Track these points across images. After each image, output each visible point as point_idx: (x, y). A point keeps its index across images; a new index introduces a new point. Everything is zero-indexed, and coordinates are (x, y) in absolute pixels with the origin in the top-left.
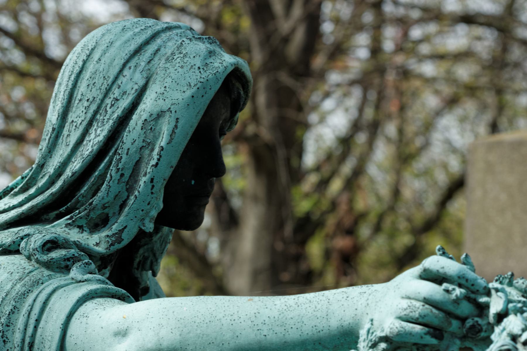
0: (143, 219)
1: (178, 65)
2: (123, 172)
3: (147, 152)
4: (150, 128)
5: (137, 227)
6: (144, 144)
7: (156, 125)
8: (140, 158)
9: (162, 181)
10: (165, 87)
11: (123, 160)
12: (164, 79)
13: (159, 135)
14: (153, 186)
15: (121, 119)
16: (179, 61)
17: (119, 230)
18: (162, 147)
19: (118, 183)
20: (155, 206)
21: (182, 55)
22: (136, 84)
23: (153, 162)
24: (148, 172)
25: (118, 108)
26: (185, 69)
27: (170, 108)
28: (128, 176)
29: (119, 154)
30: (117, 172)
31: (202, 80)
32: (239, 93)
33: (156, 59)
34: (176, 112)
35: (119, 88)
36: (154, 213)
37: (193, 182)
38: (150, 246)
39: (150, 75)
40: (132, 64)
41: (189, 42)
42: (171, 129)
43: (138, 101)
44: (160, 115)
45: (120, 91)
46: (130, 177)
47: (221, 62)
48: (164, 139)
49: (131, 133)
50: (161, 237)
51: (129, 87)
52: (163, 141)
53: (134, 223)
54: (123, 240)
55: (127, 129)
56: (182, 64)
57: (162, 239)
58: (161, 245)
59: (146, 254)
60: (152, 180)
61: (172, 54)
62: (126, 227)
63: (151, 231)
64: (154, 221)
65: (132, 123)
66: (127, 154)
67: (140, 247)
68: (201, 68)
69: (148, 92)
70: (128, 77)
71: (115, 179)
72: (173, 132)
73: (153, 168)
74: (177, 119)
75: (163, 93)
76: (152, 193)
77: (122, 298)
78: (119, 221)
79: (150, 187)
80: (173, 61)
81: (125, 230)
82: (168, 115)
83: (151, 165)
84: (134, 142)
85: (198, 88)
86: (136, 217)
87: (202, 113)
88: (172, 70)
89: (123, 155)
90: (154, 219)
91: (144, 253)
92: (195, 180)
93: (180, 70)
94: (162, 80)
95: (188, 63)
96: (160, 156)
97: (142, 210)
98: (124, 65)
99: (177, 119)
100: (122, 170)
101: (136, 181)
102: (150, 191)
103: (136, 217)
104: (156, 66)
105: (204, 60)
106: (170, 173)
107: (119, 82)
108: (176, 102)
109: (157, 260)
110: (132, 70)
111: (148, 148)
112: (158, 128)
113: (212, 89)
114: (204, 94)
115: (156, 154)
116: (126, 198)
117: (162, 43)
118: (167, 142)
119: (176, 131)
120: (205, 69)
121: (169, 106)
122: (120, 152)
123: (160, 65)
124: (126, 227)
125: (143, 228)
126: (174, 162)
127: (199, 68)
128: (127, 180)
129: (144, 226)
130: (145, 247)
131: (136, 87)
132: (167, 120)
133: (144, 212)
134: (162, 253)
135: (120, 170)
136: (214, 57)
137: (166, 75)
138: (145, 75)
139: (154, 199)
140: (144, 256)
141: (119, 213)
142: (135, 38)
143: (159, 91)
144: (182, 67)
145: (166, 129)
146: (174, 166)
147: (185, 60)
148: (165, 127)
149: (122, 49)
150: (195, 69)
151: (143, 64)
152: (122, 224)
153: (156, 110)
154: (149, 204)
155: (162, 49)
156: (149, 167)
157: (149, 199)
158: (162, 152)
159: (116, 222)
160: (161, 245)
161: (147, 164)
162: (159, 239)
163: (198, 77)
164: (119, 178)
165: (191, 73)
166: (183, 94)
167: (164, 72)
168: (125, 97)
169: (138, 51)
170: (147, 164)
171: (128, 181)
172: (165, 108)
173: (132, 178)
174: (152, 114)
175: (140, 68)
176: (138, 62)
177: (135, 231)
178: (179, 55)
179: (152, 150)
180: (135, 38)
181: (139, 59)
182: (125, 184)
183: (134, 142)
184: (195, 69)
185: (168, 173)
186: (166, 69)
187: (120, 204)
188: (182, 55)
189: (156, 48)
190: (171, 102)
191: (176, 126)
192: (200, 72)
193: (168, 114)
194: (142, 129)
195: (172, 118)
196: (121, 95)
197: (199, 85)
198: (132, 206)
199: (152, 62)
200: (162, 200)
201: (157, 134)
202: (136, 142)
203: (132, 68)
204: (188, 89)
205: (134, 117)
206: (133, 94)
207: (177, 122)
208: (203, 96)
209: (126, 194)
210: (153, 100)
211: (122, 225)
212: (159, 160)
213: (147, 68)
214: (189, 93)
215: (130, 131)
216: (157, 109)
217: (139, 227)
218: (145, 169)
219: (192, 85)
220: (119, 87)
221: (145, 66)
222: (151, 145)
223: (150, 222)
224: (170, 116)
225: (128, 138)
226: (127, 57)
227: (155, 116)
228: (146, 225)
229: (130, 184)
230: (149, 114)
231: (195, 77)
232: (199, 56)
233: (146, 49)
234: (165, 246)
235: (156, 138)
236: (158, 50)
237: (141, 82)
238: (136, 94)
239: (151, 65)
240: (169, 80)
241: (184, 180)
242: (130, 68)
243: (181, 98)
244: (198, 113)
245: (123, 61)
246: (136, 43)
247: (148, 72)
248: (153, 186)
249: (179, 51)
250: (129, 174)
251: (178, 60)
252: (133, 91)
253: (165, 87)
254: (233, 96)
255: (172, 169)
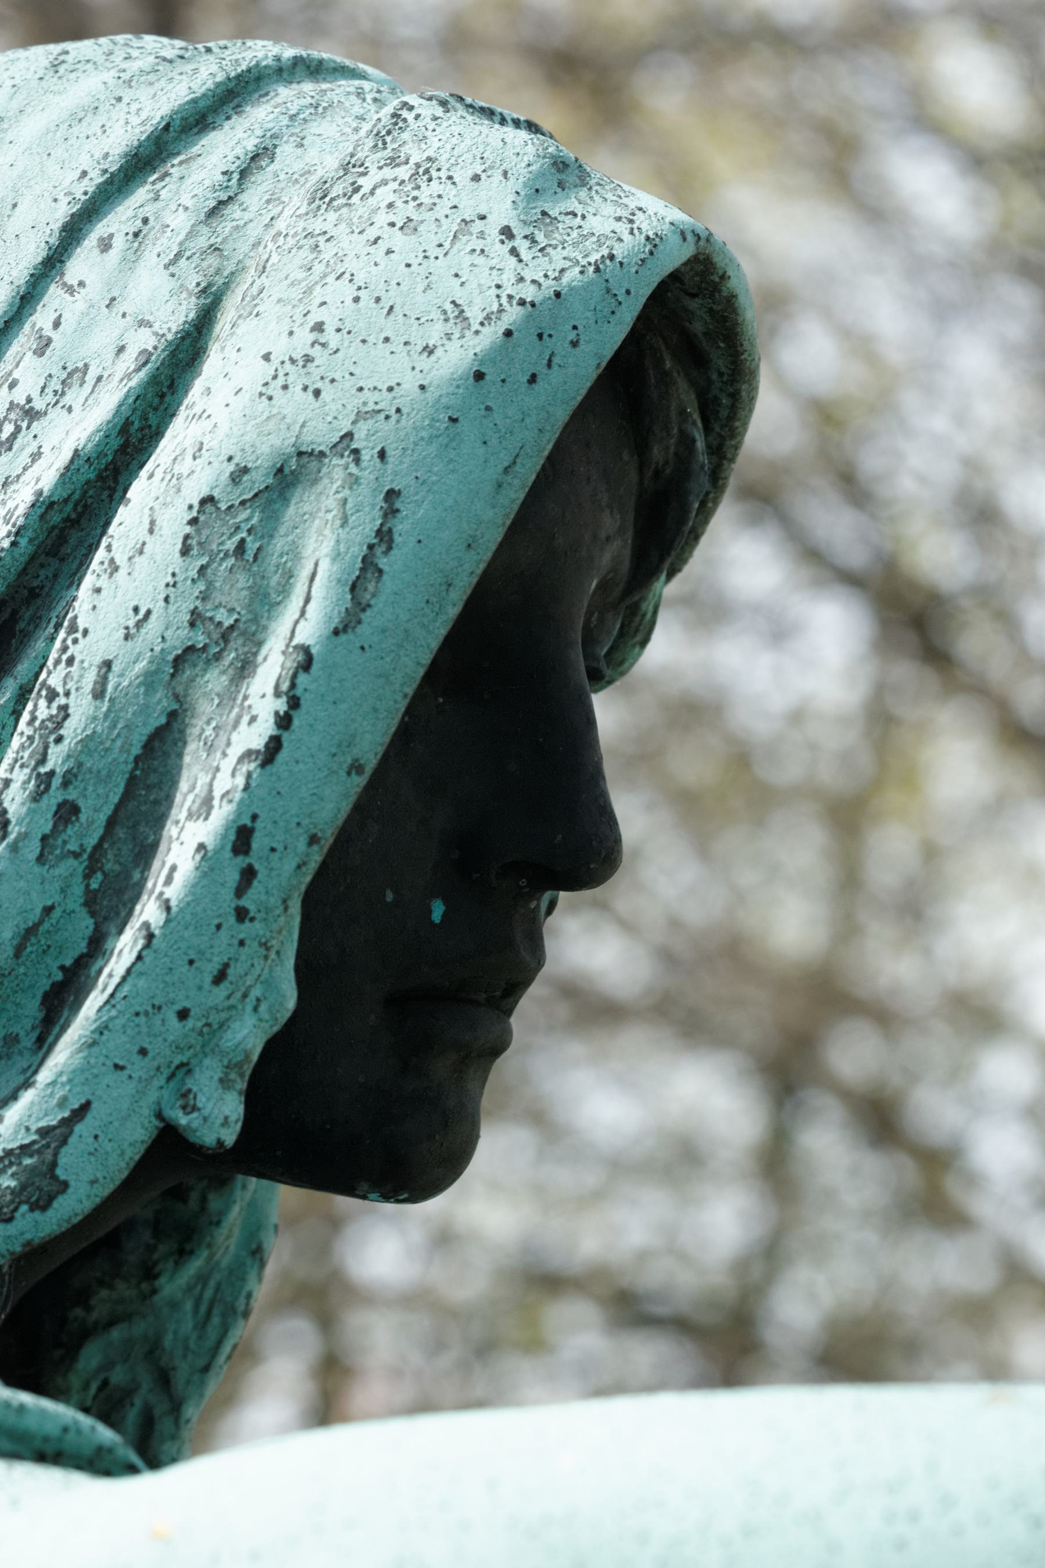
0: (185, 1068)
1: (382, 218)
2: (72, 794)
3: (215, 680)
4: (231, 545)
5: (146, 1111)
6: (200, 639)
7: (268, 528)
8: (173, 715)
9: (302, 845)
10: (319, 327)
11: (72, 729)
12: (308, 291)
13: (285, 589)
14: (249, 874)
15: (56, 518)
16: (391, 198)
17: (44, 1132)
18: (306, 650)
19: (41, 859)
20: (256, 992)
21: (404, 172)
22: (143, 323)
23: (254, 736)
24: (217, 794)
25: (36, 456)
26: (428, 237)
27: (349, 436)
28: (102, 818)
29: (52, 695)
30: (37, 797)
31: (529, 293)
32: (685, 441)
33: (253, 197)
34: (382, 455)
35: (40, 352)
36: (249, 1035)
37: (438, 911)
38: (139, 1328)
39: (220, 281)
40: (117, 221)
41: (439, 111)
42: (358, 551)
43: (153, 420)
44: (288, 476)
45: (51, 363)
46: (111, 823)
47: (625, 214)
48: (311, 608)
49: (122, 572)
50: (202, 1279)
51: (107, 332)
52: (304, 618)
53: (130, 1088)
54: (65, 1185)
55: (100, 554)
56: (404, 211)
57: (208, 1294)
58: (202, 1325)
59: (118, 1376)
60: (242, 838)
61: (346, 168)
62: (85, 1107)
63: (230, 1137)
64: (242, 1085)
65: (127, 523)
66: (98, 694)
67: (86, 1334)
68: (518, 231)
69: (212, 365)
70: (95, 291)
71: (23, 837)
72: (369, 565)
73: (252, 766)
74: (391, 495)
75: (308, 359)
76: (242, 914)
77: (99, 1464)
78: (44, 1076)
79: (233, 877)
80: (356, 198)
81: (79, 1128)
82: (339, 475)
83: (235, 751)
84: (139, 625)
85: (508, 333)
86: (143, 1052)
87: (528, 471)
88: (351, 244)
89: (72, 701)
90: (248, 1072)
91: (108, 1365)
92: (432, 923)
93: (397, 239)
94: (295, 293)
95: (441, 211)
96: (294, 703)
97: (183, 1015)
98: (73, 232)
99: (391, 495)
100: (66, 784)
101: (145, 852)
102: (227, 901)
103: (143, 1052)
104: (254, 231)
105: (529, 198)
106: (346, 807)
107: (41, 318)
108: (385, 401)
109: (176, 1408)
110: (114, 254)
111: (218, 657)
112: (279, 544)
113: (583, 346)
114: (541, 369)
115: (270, 690)
116: (82, 947)
117: (285, 121)
118: (336, 622)
119: (383, 562)
120: (540, 237)
121: (345, 426)
122: (55, 681)
123: (281, 225)
124: (85, 1107)
125: (183, 1120)
126: (372, 741)
127: (507, 232)
128: (92, 841)
129: (189, 1108)
130: (116, 1334)
131: (144, 340)
132: (331, 502)
133: (190, 1023)
134: (206, 1369)
135: (56, 782)
136: (583, 193)
137: (318, 269)
138: (193, 280)
139: (252, 947)
140: (105, 1383)
141: (41, 1040)
142: (127, 95)
143: (281, 349)
144: (408, 226)
145: (326, 548)
146: (371, 763)
147: (426, 194)
148: (320, 544)
149: (58, 153)
150: (482, 235)
151: (180, 222)
152: (60, 1093)
153: (267, 448)
154: (220, 978)
155: (286, 151)
156: (227, 765)
157: (221, 948)
158: (302, 678)
159: (27, 1084)
160: (202, 1325)
161: (210, 748)
162: (190, 1289)
163: (508, 279)
164: (47, 828)
165: (461, 257)
166: (424, 362)
167: (305, 254)
168: (74, 396)
169: (145, 161)
170: (210, 748)
171: (98, 847)
172: (321, 435)
173: (121, 833)
174: (245, 470)
175: (168, 244)
176: (148, 211)
177: (136, 1135)
178: (388, 173)
179: (245, 668)
180: (127, 95)
181: (156, 199)
182: (78, 866)
183: (139, 625)
184: (482, 235)
185: (332, 802)
186: (314, 240)
187: (45, 985)
188: (404, 172)
189: (251, 144)
190: (355, 402)
191: (385, 536)
192: (514, 252)
193: (337, 469)
194: (185, 551)
195: (364, 490)
196: (55, 385)
197: (513, 314)
198: (126, 989)
199: (233, 212)
200: (290, 962)
201: (275, 580)
202: (154, 626)
203: (119, 243)
204: (449, 336)
205: (141, 490)
206: (128, 376)
207: (390, 511)
208: (533, 379)
209: (86, 924)
210: (245, 397)
211: (62, 1103)
212: (284, 721)
213: (202, 242)
214: (456, 356)
215: (114, 568)
216: (276, 441)
217: (159, 1116)
218: (203, 780)
219: (475, 315)
220: (43, 346)
221: (191, 234)
222: (236, 642)
223: (225, 1083)
224: (353, 481)
225: (102, 601)
226: (90, 186)
227: (259, 480)
228: (201, 1100)
229: (110, 865)
230: (231, 467)
231: (489, 280)
232: (505, 174)
233: (195, 150)
234: (225, 1330)
235: (264, 602)
236: (260, 156)
237: (174, 316)
238: (143, 374)
239: (225, 228)
240: (341, 292)
241: (390, 896)
242: (105, 245)
243: (410, 384)
244: (506, 470)
245: (62, 212)
246: (135, 120)
247: (213, 261)
248: (249, 874)
249: (388, 153)
250: (108, 810)
251: (385, 194)
252: (128, 361)
253: (319, 327)
254: (656, 453)
255: (359, 782)
